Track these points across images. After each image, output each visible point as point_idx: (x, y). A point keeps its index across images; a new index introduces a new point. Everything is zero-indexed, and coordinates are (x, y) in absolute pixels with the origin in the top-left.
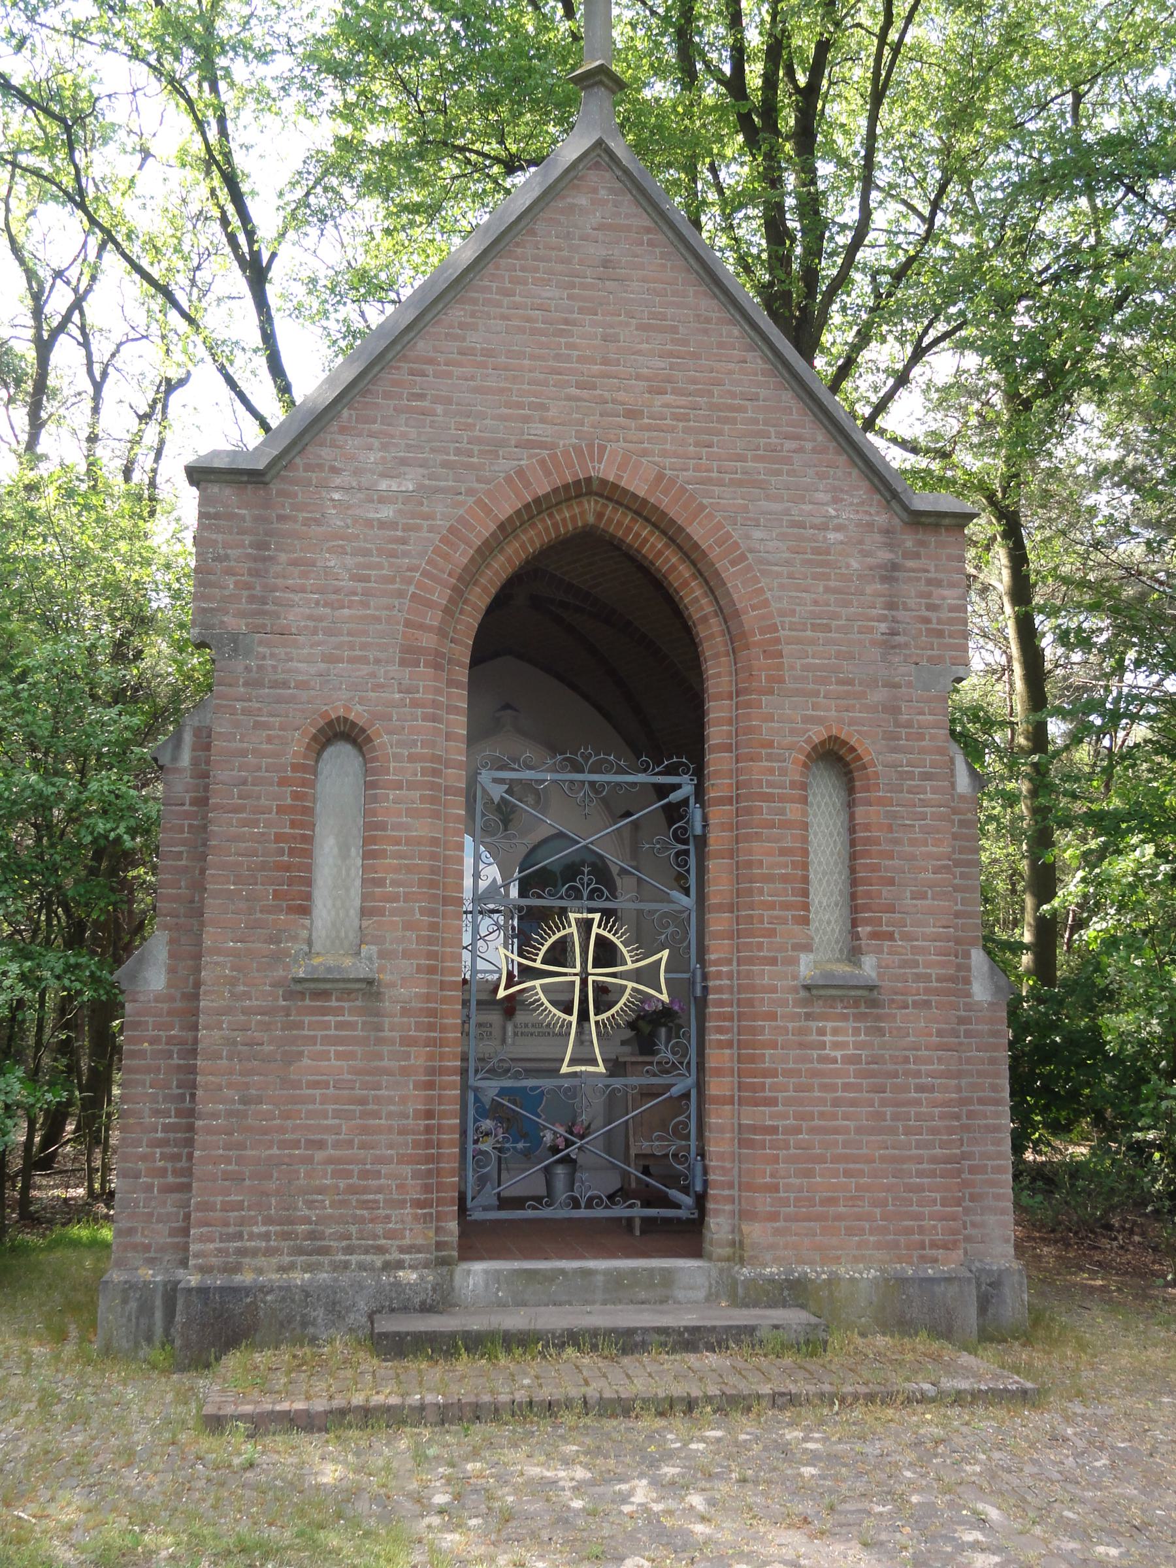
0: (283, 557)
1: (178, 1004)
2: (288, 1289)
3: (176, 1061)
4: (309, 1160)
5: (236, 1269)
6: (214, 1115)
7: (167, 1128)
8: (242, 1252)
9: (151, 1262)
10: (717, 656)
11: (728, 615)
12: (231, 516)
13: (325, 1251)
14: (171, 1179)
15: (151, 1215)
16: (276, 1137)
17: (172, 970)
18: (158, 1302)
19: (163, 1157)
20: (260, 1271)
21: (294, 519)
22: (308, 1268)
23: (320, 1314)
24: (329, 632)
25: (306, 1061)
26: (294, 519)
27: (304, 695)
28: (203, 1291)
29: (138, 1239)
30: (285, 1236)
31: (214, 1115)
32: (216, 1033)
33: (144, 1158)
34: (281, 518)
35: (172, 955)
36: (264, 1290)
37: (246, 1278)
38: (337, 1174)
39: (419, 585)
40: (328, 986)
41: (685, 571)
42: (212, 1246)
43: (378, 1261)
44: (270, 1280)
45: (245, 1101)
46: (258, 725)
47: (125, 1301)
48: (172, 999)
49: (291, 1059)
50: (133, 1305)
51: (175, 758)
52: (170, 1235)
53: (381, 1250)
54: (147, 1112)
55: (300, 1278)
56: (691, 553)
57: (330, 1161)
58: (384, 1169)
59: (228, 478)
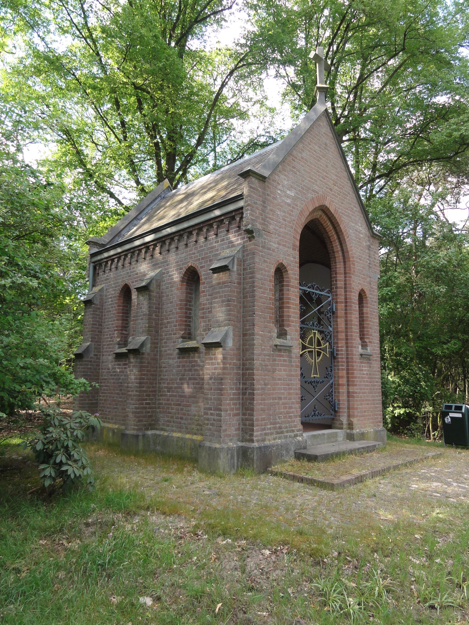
0: (269, 208)
1: (235, 352)
2: (277, 445)
3: (235, 371)
4: (278, 403)
5: (264, 440)
6: (258, 389)
7: (234, 394)
8: (266, 434)
9: (231, 440)
10: (340, 262)
11: (344, 252)
12: (257, 190)
13: (282, 432)
14: (235, 412)
15: (230, 424)
16: (272, 396)
17: (234, 340)
18: (235, 454)
19: (233, 404)
20: (269, 440)
21: (270, 196)
22: (280, 438)
23: (284, 452)
24: (279, 236)
25: (277, 372)
26: (270, 196)
27: (274, 254)
28: (260, 448)
29: (228, 433)
30: (275, 428)
31: (258, 389)
32: (258, 362)
33: (229, 404)
34: (268, 195)
35: (234, 335)
36: (273, 446)
37: (267, 443)
38: (285, 408)
39: (296, 226)
40: (282, 348)
41: (335, 237)
42: (259, 433)
43: (292, 434)
44: (277, 442)
45: (265, 384)
46: (265, 261)
47: (227, 455)
48: (233, 350)
49: (274, 371)
50: (229, 455)
51: (233, 267)
52: (235, 431)
53: (293, 431)
54: (229, 389)
55: (279, 441)
56: (338, 232)
57: (283, 404)
58: (293, 406)
59: (258, 177)
